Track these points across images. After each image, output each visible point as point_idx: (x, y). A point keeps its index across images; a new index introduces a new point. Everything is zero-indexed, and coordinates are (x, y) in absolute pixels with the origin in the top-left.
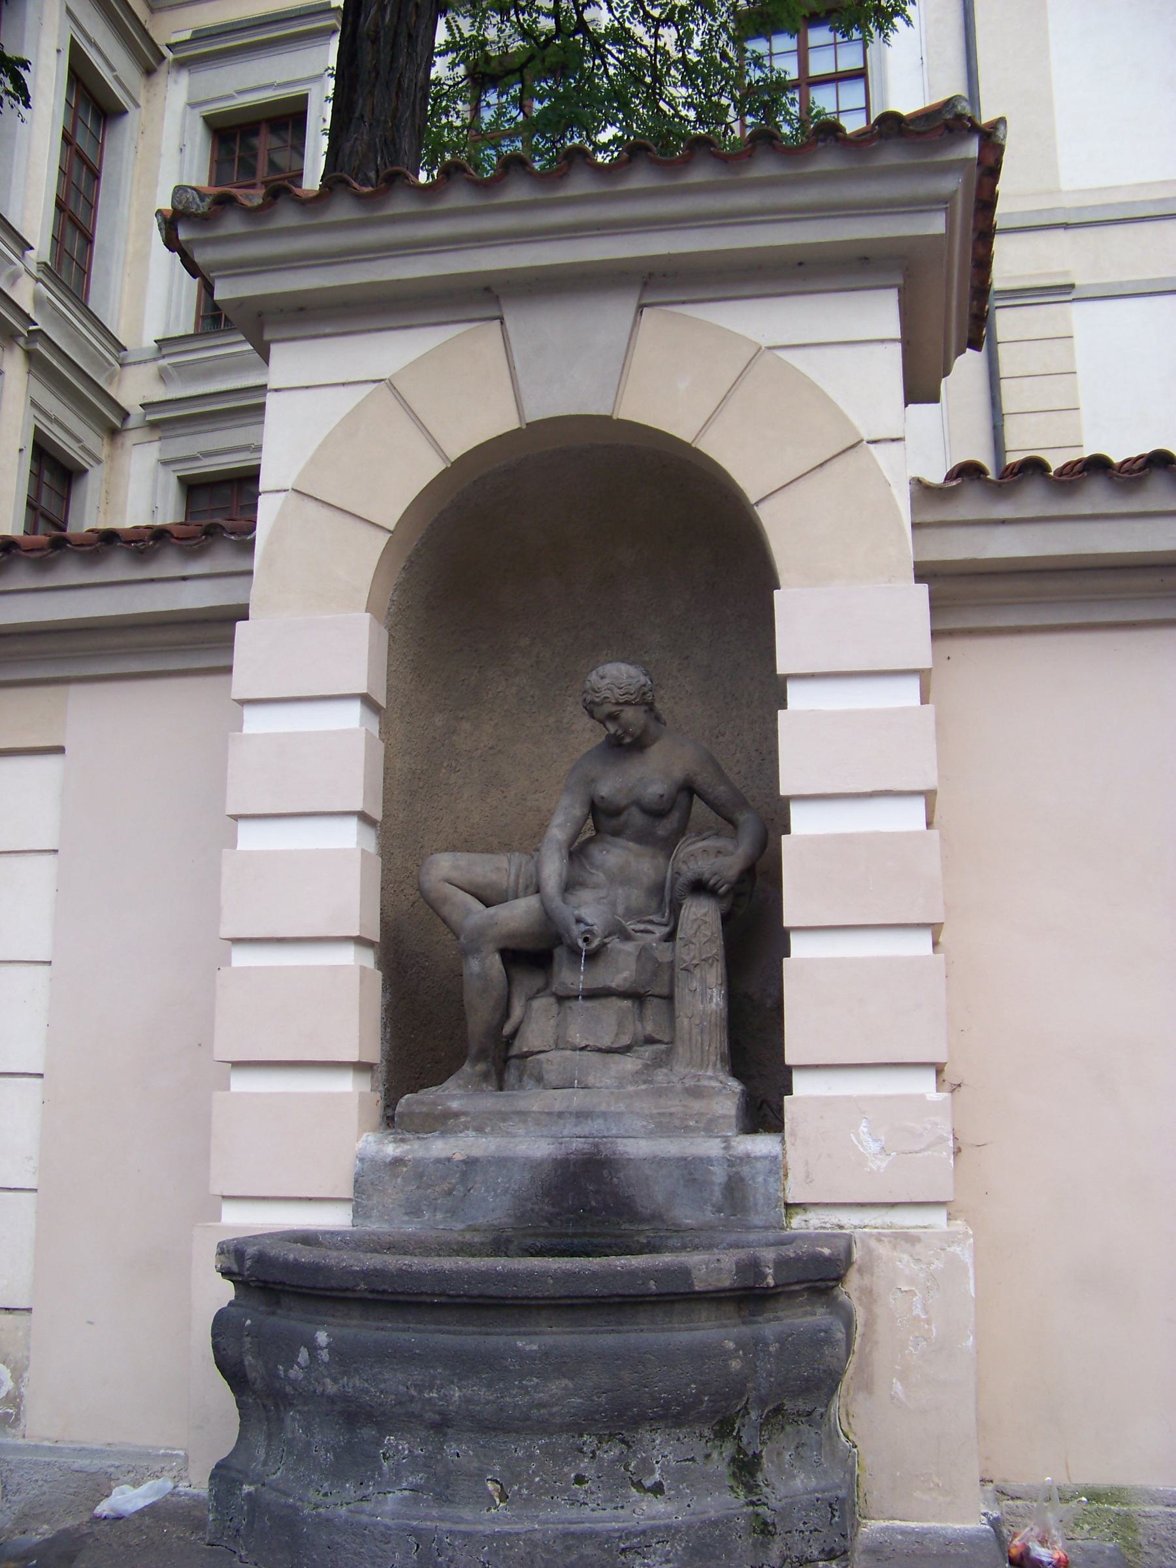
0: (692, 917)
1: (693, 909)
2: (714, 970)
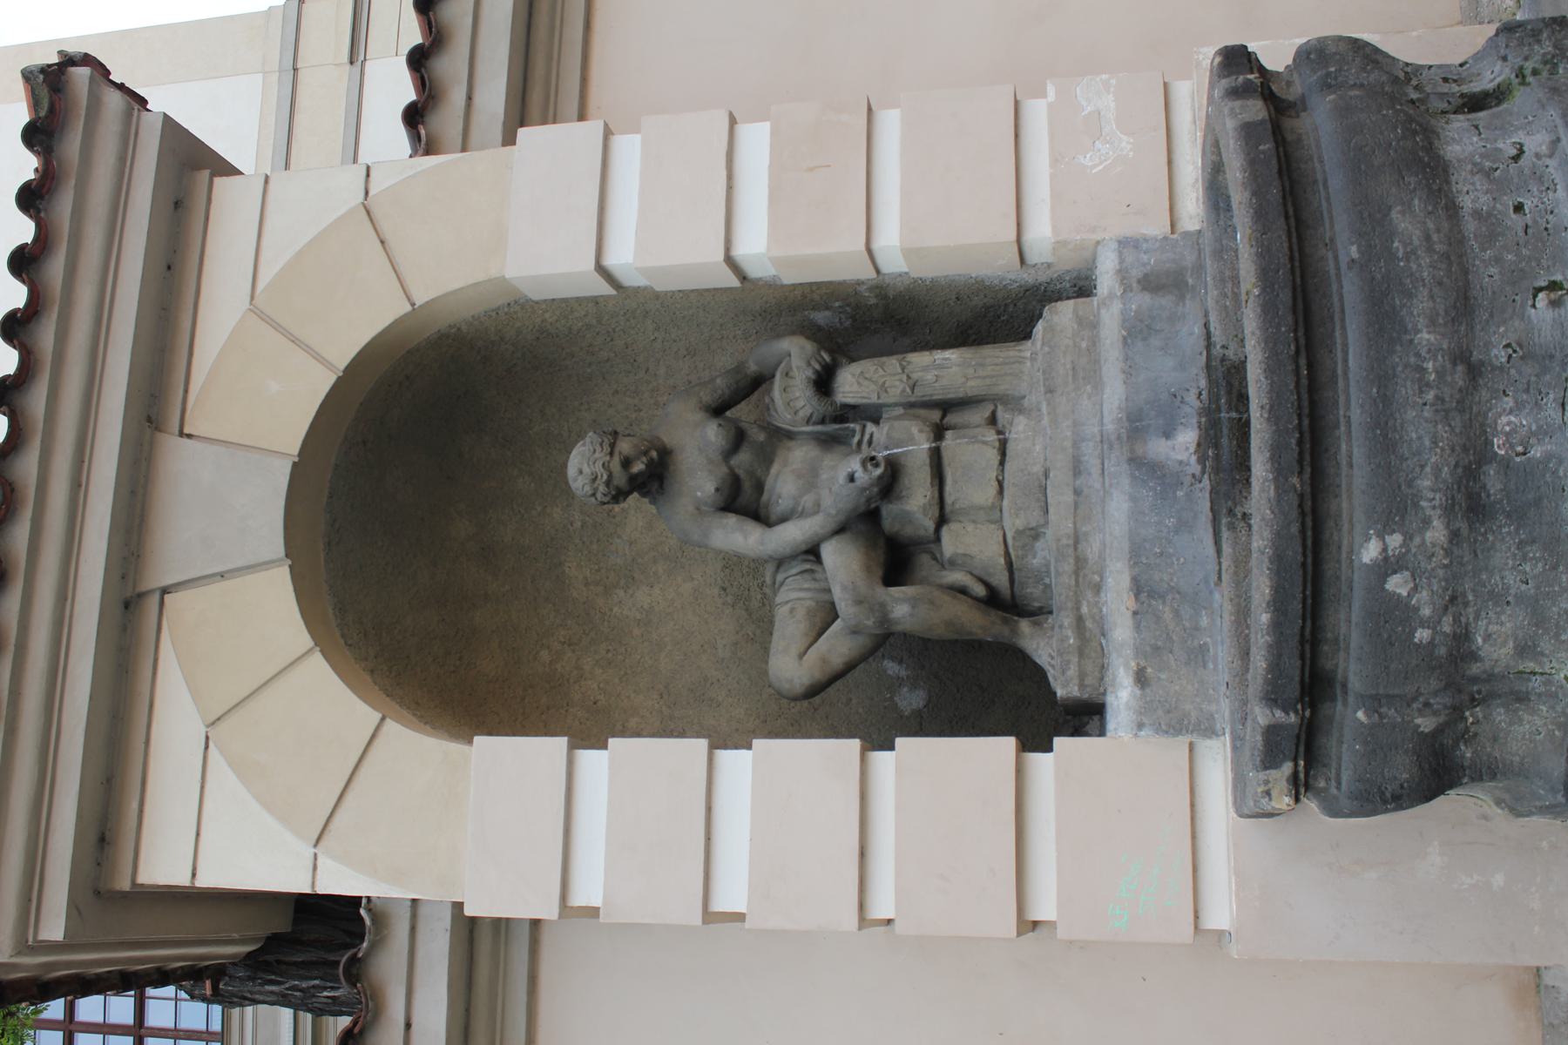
0: (855, 388)
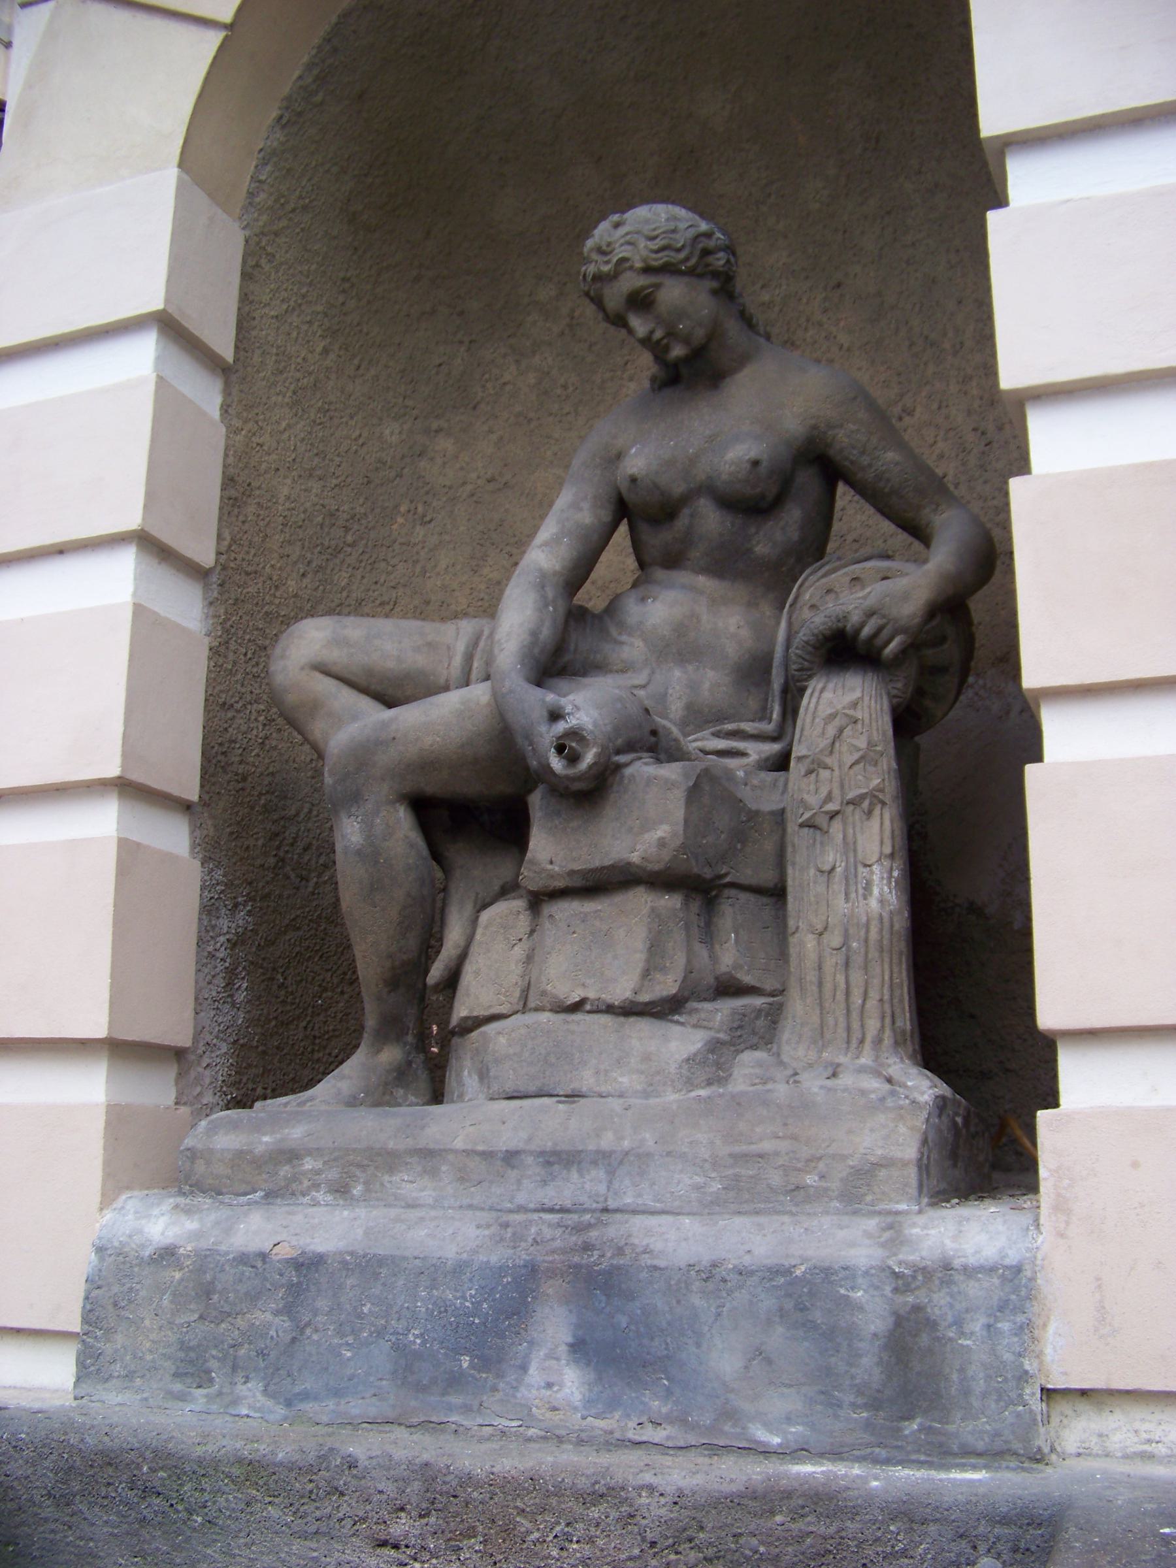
0: (825, 710)
1: (828, 695)
2: (875, 823)
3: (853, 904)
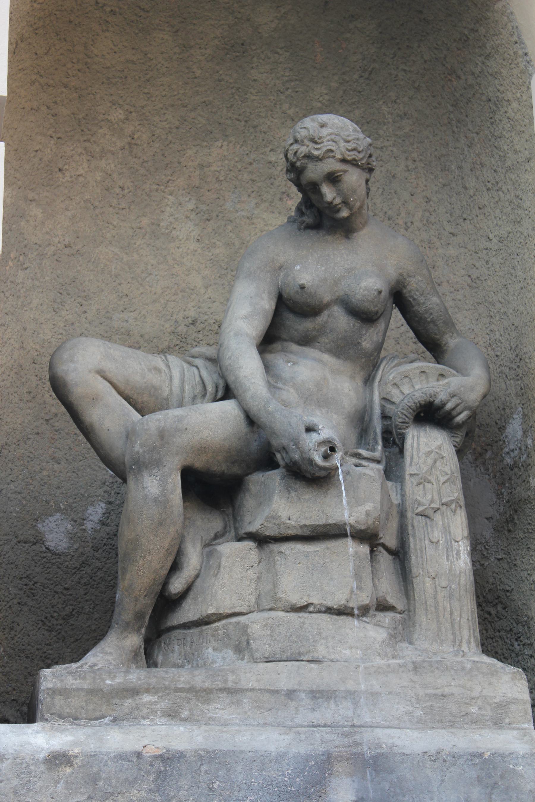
0: (424, 449)
3: (451, 563)
